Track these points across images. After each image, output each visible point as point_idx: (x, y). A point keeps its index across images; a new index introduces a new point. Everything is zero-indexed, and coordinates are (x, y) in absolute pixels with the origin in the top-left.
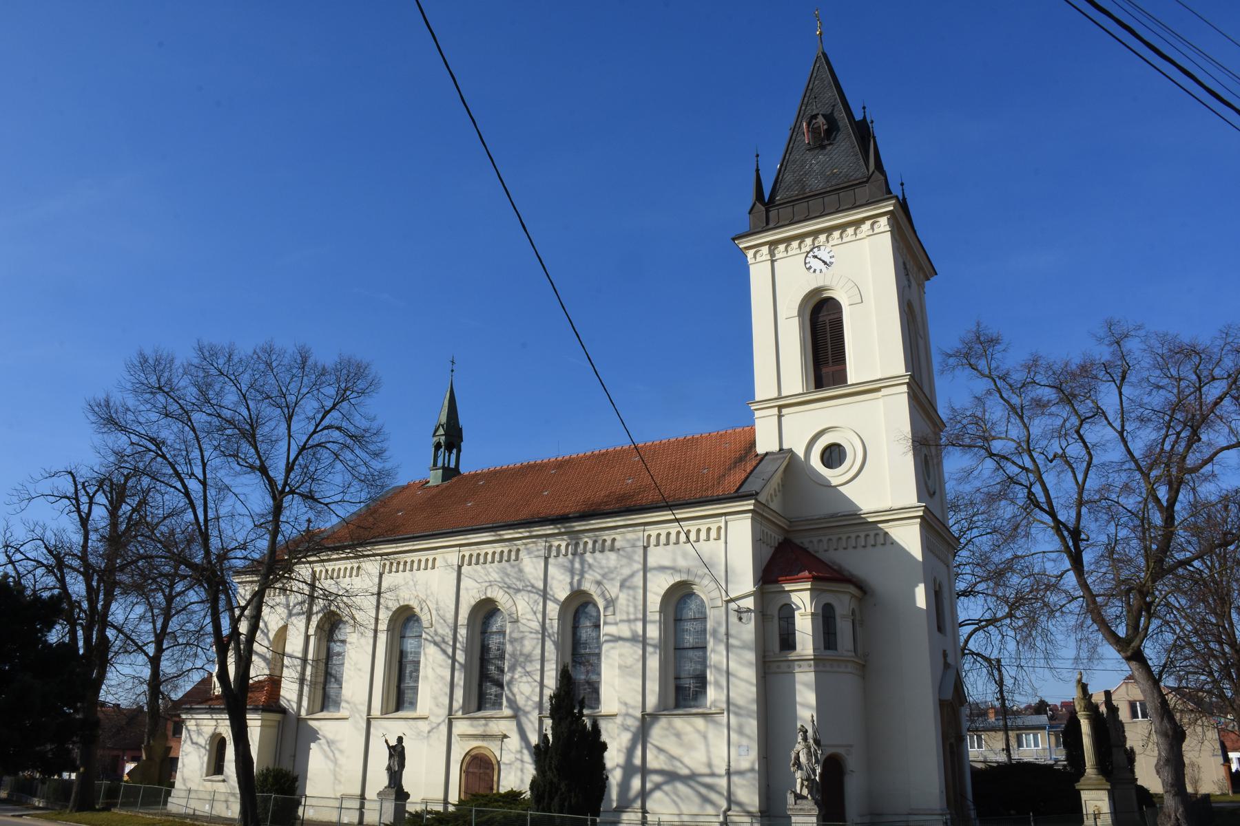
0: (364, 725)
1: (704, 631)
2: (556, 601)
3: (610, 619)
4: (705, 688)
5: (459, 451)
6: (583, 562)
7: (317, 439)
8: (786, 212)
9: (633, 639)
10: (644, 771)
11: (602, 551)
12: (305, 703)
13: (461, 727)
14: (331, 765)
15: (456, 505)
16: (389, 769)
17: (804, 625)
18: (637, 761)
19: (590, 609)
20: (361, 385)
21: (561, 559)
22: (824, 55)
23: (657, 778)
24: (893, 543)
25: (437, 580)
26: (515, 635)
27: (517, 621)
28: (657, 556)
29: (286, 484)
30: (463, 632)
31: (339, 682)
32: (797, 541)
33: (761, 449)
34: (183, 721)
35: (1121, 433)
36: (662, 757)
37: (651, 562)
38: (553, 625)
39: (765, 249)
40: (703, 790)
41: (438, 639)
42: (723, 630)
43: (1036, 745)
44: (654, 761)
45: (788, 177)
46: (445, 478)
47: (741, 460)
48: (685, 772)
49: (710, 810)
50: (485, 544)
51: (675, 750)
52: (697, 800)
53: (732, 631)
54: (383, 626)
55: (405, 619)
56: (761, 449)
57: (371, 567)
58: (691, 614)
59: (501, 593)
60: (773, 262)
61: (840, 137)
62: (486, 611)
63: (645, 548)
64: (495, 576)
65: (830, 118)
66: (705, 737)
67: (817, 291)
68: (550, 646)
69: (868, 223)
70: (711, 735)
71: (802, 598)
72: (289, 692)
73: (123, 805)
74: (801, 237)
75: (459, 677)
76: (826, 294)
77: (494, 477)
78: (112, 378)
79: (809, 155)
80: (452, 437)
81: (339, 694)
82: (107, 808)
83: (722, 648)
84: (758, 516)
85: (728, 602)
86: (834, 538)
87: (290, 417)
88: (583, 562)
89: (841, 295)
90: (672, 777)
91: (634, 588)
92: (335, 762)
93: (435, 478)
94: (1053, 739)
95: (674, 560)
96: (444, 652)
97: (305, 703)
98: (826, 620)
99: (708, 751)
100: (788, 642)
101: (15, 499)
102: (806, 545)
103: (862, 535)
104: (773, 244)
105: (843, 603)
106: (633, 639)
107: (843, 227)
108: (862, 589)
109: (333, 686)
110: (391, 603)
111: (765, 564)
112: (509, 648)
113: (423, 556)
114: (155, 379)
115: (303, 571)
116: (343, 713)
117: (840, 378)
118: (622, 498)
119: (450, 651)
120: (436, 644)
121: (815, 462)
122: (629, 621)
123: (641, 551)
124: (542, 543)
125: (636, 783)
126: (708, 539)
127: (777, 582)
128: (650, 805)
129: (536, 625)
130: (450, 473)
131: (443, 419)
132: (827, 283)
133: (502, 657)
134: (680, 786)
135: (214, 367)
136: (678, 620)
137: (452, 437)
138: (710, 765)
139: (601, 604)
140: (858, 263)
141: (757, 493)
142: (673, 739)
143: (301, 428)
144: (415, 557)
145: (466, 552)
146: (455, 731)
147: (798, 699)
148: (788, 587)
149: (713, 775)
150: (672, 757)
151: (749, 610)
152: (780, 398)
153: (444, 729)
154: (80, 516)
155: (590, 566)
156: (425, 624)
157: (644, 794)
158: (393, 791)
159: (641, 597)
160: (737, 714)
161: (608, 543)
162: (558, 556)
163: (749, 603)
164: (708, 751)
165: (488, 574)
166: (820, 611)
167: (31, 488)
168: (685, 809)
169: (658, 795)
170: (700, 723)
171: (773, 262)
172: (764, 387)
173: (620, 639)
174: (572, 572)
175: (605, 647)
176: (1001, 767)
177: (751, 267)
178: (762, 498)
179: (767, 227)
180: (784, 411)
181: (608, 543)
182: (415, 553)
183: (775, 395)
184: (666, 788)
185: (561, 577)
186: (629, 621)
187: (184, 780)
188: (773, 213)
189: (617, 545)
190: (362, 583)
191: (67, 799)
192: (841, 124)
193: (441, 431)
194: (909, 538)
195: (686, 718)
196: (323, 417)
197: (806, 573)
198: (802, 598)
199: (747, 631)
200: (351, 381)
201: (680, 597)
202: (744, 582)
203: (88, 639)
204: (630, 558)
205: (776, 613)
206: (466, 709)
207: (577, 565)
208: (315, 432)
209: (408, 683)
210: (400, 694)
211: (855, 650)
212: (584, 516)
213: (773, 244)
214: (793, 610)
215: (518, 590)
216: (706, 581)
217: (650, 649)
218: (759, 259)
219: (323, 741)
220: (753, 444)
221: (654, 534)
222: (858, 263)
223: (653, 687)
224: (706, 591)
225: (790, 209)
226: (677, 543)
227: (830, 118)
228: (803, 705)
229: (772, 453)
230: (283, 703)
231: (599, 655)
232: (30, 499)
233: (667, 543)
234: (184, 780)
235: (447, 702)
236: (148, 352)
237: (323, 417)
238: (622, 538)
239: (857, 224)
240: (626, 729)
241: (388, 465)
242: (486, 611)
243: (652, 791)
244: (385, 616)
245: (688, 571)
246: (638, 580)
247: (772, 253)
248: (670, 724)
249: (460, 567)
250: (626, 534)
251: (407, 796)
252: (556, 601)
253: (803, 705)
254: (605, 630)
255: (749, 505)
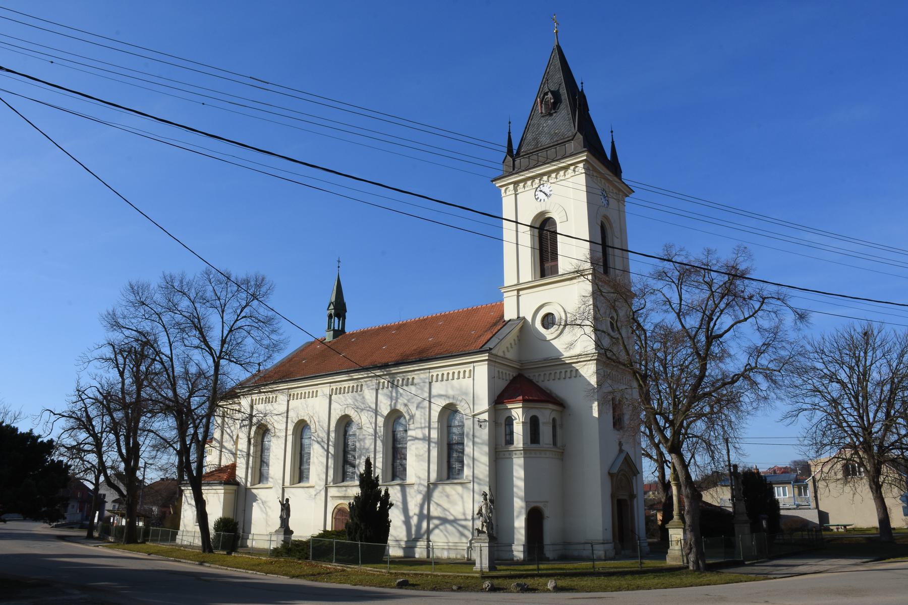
0: (281, 491)
1: (463, 434)
2: (382, 416)
3: (412, 426)
4: (463, 467)
5: (344, 318)
6: (397, 392)
7: (239, 324)
8: (525, 161)
9: (423, 439)
10: (429, 518)
11: (407, 385)
12: (249, 479)
13: (333, 492)
14: (264, 516)
15: (341, 353)
16: (281, 517)
17: (518, 429)
18: (425, 512)
19: (402, 421)
20: (264, 289)
21: (385, 390)
22: (559, 47)
23: (437, 522)
24: (581, 376)
25: (317, 403)
26: (361, 437)
27: (361, 428)
28: (437, 388)
29: (221, 352)
30: (333, 435)
31: (268, 465)
32: (526, 375)
33: (506, 318)
34: (182, 491)
35: (678, 315)
36: (439, 509)
37: (434, 392)
38: (381, 431)
39: (511, 187)
40: (461, 529)
41: (319, 440)
42: (471, 433)
43: (785, 494)
44: (435, 511)
45: (529, 136)
46: (334, 337)
47: (495, 324)
48: (451, 518)
49: (464, 540)
50: (343, 381)
51: (446, 505)
52: (457, 534)
53: (477, 434)
54: (290, 432)
55: (302, 427)
56: (506, 318)
57: (282, 398)
58: (456, 423)
59: (353, 411)
60: (516, 195)
61: (562, 106)
62: (345, 422)
63: (430, 383)
64: (350, 401)
65: (556, 94)
66: (462, 498)
67: (542, 213)
68: (379, 444)
69: (572, 168)
70: (465, 496)
71: (517, 412)
72: (240, 473)
73: (152, 541)
74: (533, 178)
75: (331, 462)
76: (547, 216)
77: (364, 335)
78: (115, 298)
79: (542, 121)
80: (339, 309)
81: (268, 473)
82: (144, 542)
83: (471, 444)
84: (492, 362)
85: (474, 416)
86: (548, 373)
87: (223, 312)
88: (397, 392)
89: (555, 215)
90: (444, 521)
91: (424, 408)
92: (267, 514)
93: (329, 337)
94: (796, 490)
95: (447, 391)
96: (323, 447)
97: (249, 479)
98: (533, 426)
99: (464, 506)
100: (510, 441)
101: (80, 362)
102: (531, 378)
103: (563, 371)
104: (516, 184)
105: (546, 414)
106: (423, 439)
107: (557, 171)
108: (560, 404)
109: (265, 468)
110: (294, 417)
111: (498, 393)
112: (358, 445)
113: (310, 389)
114: (139, 297)
115: (245, 402)
116: (270, 484)
117: (554, 271)
118: (422, 351)
119: (326, 447)
120: (318, 442)
121: (538, 325)
122: (421, 428)
123: (427, 385)
124: (375, 381)
125: (425, 525)
126: (464, 377)
127: (503, 403)
128: (432, 537)
129: (371, 431)
130: (339, 333)
131: (333, 299)
132: (547, 208)
133: (354, 450)
134: (449, 526)
135: (174, 288)
136: (449, 427)
137: (339, 309)
138: (464, 514)
139: (407, 417)
140: (565, 195)
141: (491, 349)
142: (445, 498)
143: (229, 317)
144: (299, 391)
145: (334, 386)
146: (329, 494)
147: (515, 474)
148: (509, 406)
149: (466, 520)
150: (445, 509)
151: (485, 421)
152: (518, 284)
153: (323, 493)
154: (119, 370)
155: (401, 395)
156: (313, 430)
157: (429, 532)
158: (283, 530)
159: (427, 413)
160: (479, 484)
161: (410, 380)
162: (383, 388)
163: (485, 416)
164: (464, 506)
165: (346, 400)
166: (528, 421)
167: (89, 355)
168: (451, 539)
169: (437, 531)
170: (459, 488)
171: (516, 195)
172: (509, 278)
173: (416, 438)
174: (391, 398)
175: (409, 443)
176: (779, 507)
177: (504, 199)
178: (493, 352)
179: (514, 171)
180: (521, 293)
181: (410, 380)
182: (302, 388)
183: (516, 282)
184: (441, 527)
185: (385, 402)
186: (421, 428)
187: (185, 526)
188: (517, 162)
189: (415, 381)
190: (280, 408)
191: (122, 537)
192: (563, 98)
193: (332, 307)
194: (589, 372)
195: (451, 486)
196: (241, 312)
197: (521, 398)
198: (517, 412)
199: (484, 434)
200: (254, 290)
201: (450, 411)
202: (483, 404)
203: (127, 444)
204: (422, 389)
205: (503, 422)
206: (335, 481)
207: (394, 394)
208: (237, 320)
209: (305, 466)
210: (300, 474)
211: (555, 443)
212: (397, 364)
213: (516, 184)
214: (512, 420)
215: (362, 410)
216: (463, 404)
217: (433, 445)
218: (508, 193)
219: (259, 501)
220: (503, 316)
221: (435, 374)
222: (565, 195)
223: (434, 467)
224: (463, 408)
225: (553, 150)
226: (447, 380)
227: (556, 94)
228: (518, 478)
229: (513, 320)
230: (238, 479)
231: (406, 448)
232: (89, 362)
233: (442, 380)
234: (185, 526)
235: (324, 477)
236: (134, 283)
237: (241, 312)
238: (419, 377)
239: (566, 168)
240: (420, 492)
241: (282, 337)
242: (345, 422)
243: (433, 529)
244: (291, 427)
245: (453, 397)
246: (426, 403)
247: (515, 189)
248: (443, 489)
249: (331, 396)
250: (419, 374)
251: (292, 532)
252: (382, 416)
253: (518, 478)
254: (410, 433)
255: (485, 356)
